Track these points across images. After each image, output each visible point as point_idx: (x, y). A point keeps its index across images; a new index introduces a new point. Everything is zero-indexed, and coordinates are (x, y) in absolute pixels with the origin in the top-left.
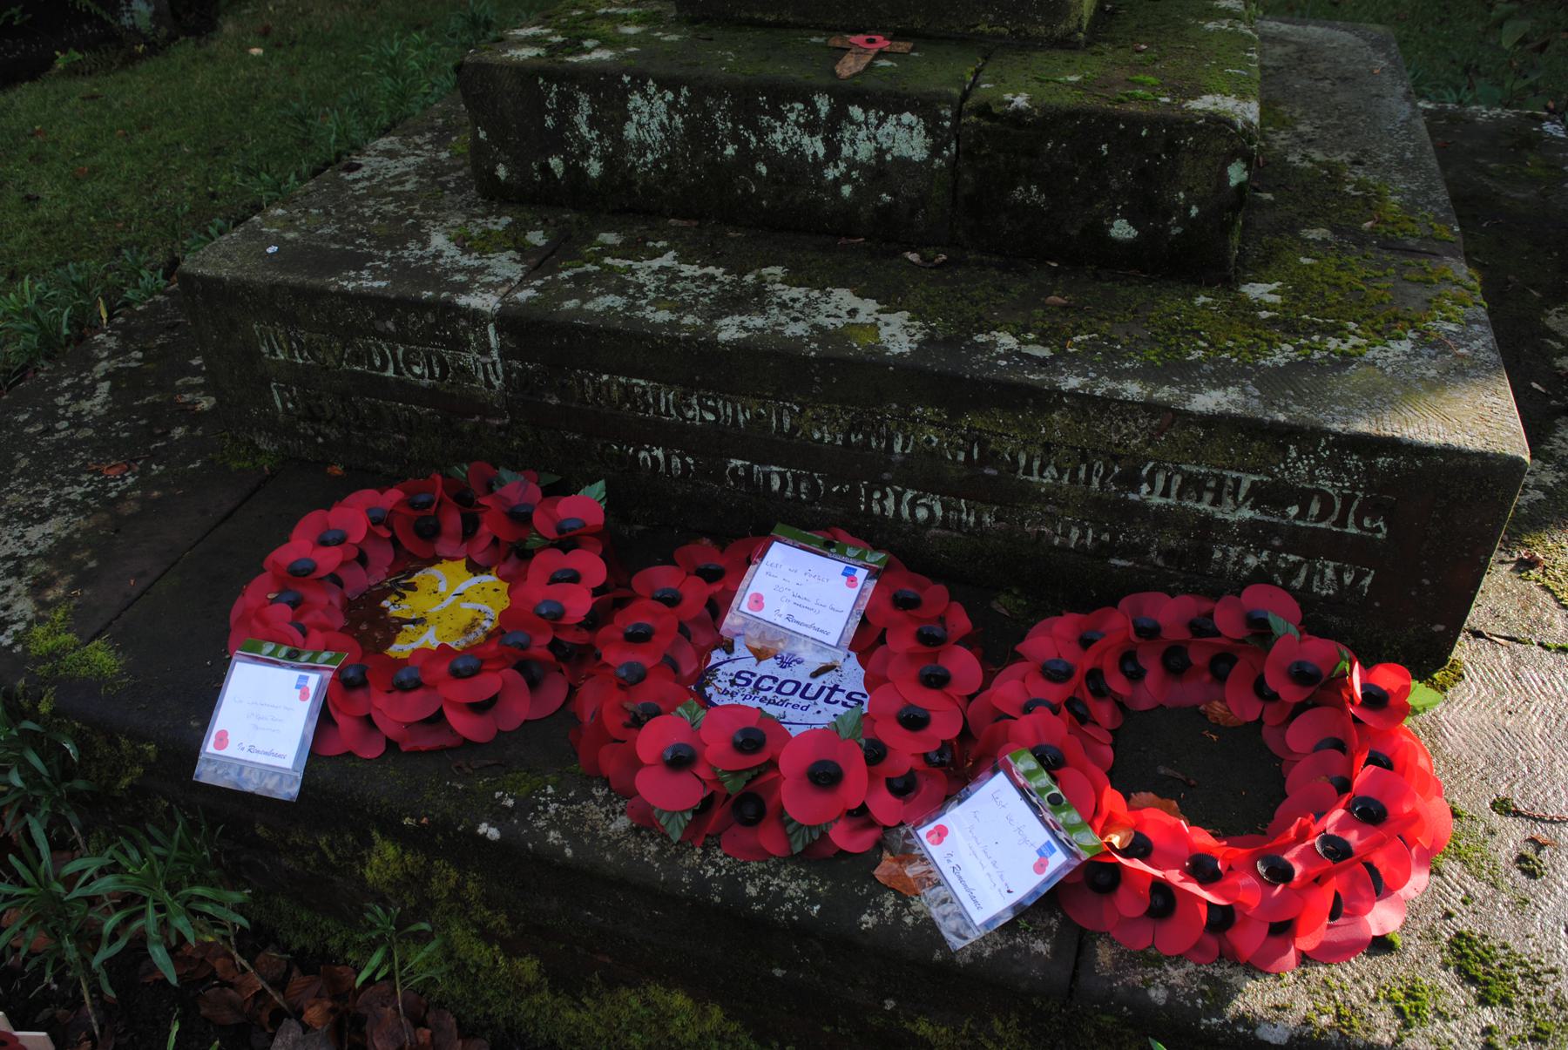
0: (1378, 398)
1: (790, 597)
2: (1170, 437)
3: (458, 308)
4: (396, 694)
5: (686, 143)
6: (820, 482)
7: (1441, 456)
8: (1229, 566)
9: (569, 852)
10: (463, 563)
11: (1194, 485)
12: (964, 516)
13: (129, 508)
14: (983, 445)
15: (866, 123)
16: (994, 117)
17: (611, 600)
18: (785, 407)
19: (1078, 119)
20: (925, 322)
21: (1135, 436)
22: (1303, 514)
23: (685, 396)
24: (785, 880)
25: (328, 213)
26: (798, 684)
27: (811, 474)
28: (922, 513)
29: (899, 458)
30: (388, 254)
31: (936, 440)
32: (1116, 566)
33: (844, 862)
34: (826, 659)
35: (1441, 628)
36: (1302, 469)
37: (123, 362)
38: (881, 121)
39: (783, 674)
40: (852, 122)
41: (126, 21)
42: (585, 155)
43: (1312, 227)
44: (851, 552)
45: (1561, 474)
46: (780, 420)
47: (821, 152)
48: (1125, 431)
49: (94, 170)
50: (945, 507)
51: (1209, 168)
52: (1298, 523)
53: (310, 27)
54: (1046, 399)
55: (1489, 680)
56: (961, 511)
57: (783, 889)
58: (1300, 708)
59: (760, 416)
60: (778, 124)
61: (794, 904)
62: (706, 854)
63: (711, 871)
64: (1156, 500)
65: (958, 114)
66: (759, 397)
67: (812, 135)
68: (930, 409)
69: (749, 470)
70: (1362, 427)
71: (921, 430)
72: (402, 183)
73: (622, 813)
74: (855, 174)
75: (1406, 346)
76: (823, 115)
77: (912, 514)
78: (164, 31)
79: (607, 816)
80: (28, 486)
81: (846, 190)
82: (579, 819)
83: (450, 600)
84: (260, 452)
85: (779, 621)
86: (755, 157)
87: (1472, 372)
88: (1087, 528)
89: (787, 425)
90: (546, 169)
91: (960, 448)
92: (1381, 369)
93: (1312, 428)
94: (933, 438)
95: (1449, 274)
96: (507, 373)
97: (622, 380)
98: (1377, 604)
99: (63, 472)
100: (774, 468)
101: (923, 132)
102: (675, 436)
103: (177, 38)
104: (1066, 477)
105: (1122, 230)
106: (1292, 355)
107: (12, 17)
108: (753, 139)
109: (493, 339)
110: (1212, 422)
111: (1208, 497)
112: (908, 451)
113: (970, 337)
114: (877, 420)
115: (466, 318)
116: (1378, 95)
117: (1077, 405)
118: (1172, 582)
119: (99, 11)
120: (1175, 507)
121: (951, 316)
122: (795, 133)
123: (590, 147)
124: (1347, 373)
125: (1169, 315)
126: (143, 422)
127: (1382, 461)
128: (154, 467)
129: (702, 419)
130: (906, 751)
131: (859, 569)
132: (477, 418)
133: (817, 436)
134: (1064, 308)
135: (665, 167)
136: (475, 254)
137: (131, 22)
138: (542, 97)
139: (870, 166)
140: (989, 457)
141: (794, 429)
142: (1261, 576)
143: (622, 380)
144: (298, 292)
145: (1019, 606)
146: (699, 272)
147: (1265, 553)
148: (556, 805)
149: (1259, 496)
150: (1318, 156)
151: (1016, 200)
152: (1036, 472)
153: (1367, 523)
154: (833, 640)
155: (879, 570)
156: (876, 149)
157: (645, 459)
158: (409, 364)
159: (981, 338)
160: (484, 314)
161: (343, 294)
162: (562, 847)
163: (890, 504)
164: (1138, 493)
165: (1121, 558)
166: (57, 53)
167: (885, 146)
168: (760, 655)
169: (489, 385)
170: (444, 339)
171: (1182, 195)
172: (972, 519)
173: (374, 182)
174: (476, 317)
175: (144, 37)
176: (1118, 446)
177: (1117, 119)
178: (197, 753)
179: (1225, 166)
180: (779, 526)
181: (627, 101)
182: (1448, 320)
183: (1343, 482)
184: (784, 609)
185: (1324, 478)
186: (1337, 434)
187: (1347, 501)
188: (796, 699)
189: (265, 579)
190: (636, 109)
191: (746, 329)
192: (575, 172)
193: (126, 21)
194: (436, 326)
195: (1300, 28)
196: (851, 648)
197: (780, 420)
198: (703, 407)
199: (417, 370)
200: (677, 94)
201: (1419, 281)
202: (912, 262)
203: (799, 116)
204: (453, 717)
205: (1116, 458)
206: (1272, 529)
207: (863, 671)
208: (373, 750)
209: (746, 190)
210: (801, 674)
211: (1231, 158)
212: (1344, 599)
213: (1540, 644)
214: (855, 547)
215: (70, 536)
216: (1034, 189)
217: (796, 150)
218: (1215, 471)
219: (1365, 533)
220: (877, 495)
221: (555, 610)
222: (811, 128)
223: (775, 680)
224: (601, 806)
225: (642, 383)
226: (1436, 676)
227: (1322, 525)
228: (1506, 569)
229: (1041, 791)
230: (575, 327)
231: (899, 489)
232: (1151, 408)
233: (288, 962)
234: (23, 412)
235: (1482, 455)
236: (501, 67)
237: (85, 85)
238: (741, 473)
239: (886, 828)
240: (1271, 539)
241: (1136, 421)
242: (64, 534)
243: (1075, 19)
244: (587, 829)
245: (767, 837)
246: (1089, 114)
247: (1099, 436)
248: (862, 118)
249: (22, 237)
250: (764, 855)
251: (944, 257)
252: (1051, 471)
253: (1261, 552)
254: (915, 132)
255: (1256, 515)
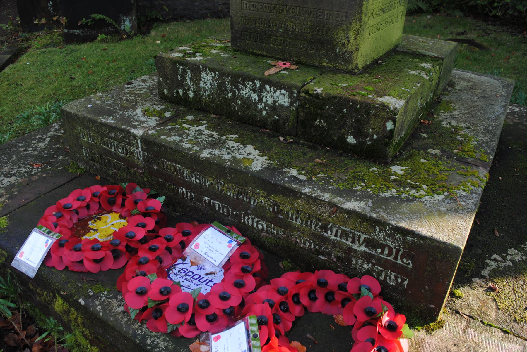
0: (417, 215)
1: (208, 247)
2: (336, 216)
3: (130, 133)
4: (73, 251)
5: (217, 90)
6: (230, 209)
7: (430, 241)
8: (358, 267)
9: (101, 314)
10: (119, 214)
11: (345, 234)
12: (273, 230)
13: (34, 178)
14: (278, 207)
15: (271, 92)
16: (310, 95)
17: (153, 234)
18: (219, 182)
19: (336, 99)
20: (271, 161)
21: (325, 213)
22: (382, 252)
23: (191, 173)
24: (161, 341)
25: (113, 97)
26: (200, 276)
27: (227, 207)
28: (260, 227)
29: (253, 206)
30: (121, 112)
31: (264, 202)
32: (321, 258)
33: (182, 340)
34: (213, 270)
35: (433, 306)
36: (381, 235)
37: (57, 133)
38: (275, 91)
39: (197, 272)
40: (266, 91)
41: (122, 27)
42: (189, 90)
43: (434, 149)
44: (234, 235)
45: (524, 258)
46: (218, 186)
47: (257, 99)
48: (322, 211)
49: (94, 72)
50: (267, 226)
51: (380, 122)
52: (381, 256)
53: (178, 36)
54: (296, 195)
55: (453, 330)
56: (272, 229)
57: (158, 344)
58: (364, 325)
59: (212, 184)
60: (244, 88)
61: (159, 350)
62: (141, 325)
63: (140, 331)
64: (333, 238)
65: (299, 92)
66: (212, 177)
67: (254, 93)
68: (261, 191)
69: (209, 201)
70: (403, 224)
71: (259, 198)
72: (140, 91)
73: (123, 306)
74: (267, 108)
75: (441, 197)
76: (257, 87)
77: (257, 226)
78: (133, 32)
79: (118, 305)
80: (11, 166)
81: (264, 113)
82: (109, 304)
83: (109, 225)
84: (79, 168)
85: (202, 254)
86: (237, 98)
87: (461, 212)
88: (311, 243)
89: (220, 189)
90: (178, 92)
91: (270, 206)
92: (425, 204)
93: (384, 222)
94: (263, 201)
95: (476, 174)
96: (144, 156)
97: (174, 164)
98: (410, 292)
99: (23, 164)
100: (217, 202)
101: (288, 97)
102: (189, 186)
103: (137, 35)
104: (304, 223)
105: (351, 140)
106: (394, 194)
107: (88, 22)
108: (237, 92)
109: (140, 145)
110: (350, 213)
111: (350, 240)
112: (255, 204)
113: (282, 168)
114: (246, 192)
115: (133, 136)
116: (493, 104)
117: (306, 199)
118: (340, 268)
119: (114, 23)
120: (339, 241)
121: (280, 161)
122: (249, 92)
123: (190, 87)
124: (411, 204)
125: (357, 172)
126: (53, 152)
127: (409, 239)
128: (48, 167)
129: (196, 181)
130: (217, 306)
131: (234, 242)
132: (136, 169)
133: (229, 194)
134: (321, 164)
135: (211, 97)
136: (146, 117)
137: (124, 28)
138: (177, 70)
139: (271, 106)
140: (280, 212)
141: (222, 190)
142: (369, 272)
143: (174, 164)
144: (90, 120)
145: (288, 266)
146: (210, 133)
147: (370, 264)
148: (105, 298)
149: (368, 243)
150: (454, 123)
151: (317, 124)
152: (294, 220)
153: (405, 260)
154: (217, 264)
155: (241, 243)
156: (273, 101)
157: (181, 192)
158: (118, 148)
159: (285, 170)
160: (137, 136)
161: (101, 123)
162: (100, 312)
163: (250, 221)
164: (328, 234)
165: (323, 256)
166: (99, 35)
167: (276, 100)
168: (192, 264)
169: (139, 159)
170: (127, 142)
171: (371, 130)
172: (275, 232)
173: (133, 89)
174: (135, 136)
175: (127, 33)
176: (320, 215)
177: (349, 101)
178: (14, 257)
179: (385, 122)
180: (216, 222)
181: (201, 74)
182: (464, 190)
183: (395, 243)
184: (205, 250)
185: (388, 241)
186: (392, 225)
187: (398, 251)
188: (196, 281)
189: (53, 207)
190: (203, 77)
191: (211, 154)
192: (186, 95)
193: (122, 27)
194: (124, 137)
195: (479, 77)
196: (223, 267)
197: (218, 186)
198: (196, 178)
199: (120, 150)
200: (215, 74)
201: (462, 174)
202: (280, 140)
203: (250, 86)
204: (86, 262)
205: (320, 220)
206: (372, 256)
207: (223, 277)
208: (61, 268)
209: (234, 108)
210: (202, 273)
211: (388, 119)
212: (397, 288)
213: (482, 321)
214: (237, 234)
215: (14, 183)
216: (322, 121)
217: (249, 97)
218: (352, 231)
219: (404, 264)
220: (247, 218)
221: (133, 235)
222: (254, 90)
223: (193, 273)
224: (118, 302)
225: (179, 166)
226: (431, 324)
227: (390, 258)
228: (481, 290)
229: (252, 331)
230: (161, 144)
231: (253, 217)
232: (330, 204)
233: (37, 330)
234: (22, 143)
235: (445, 243)
236: (167, 59)
237: (104, 45)
238: (207, 202)
239: (201, 332)
240: (372, 260)
241: (325, 208)
242: (13, 182)
243: (354, 65)
244: (110, 308)
245: (159, 324)
246: (341, 98)
247: (314, 211)
248: (269, 90)
249: (64, 90)
250: (158, 331)
251: (292, 140)
252: (299, 220)
253: (369, 264)
254: (285, 96)
255: (366, 250)
